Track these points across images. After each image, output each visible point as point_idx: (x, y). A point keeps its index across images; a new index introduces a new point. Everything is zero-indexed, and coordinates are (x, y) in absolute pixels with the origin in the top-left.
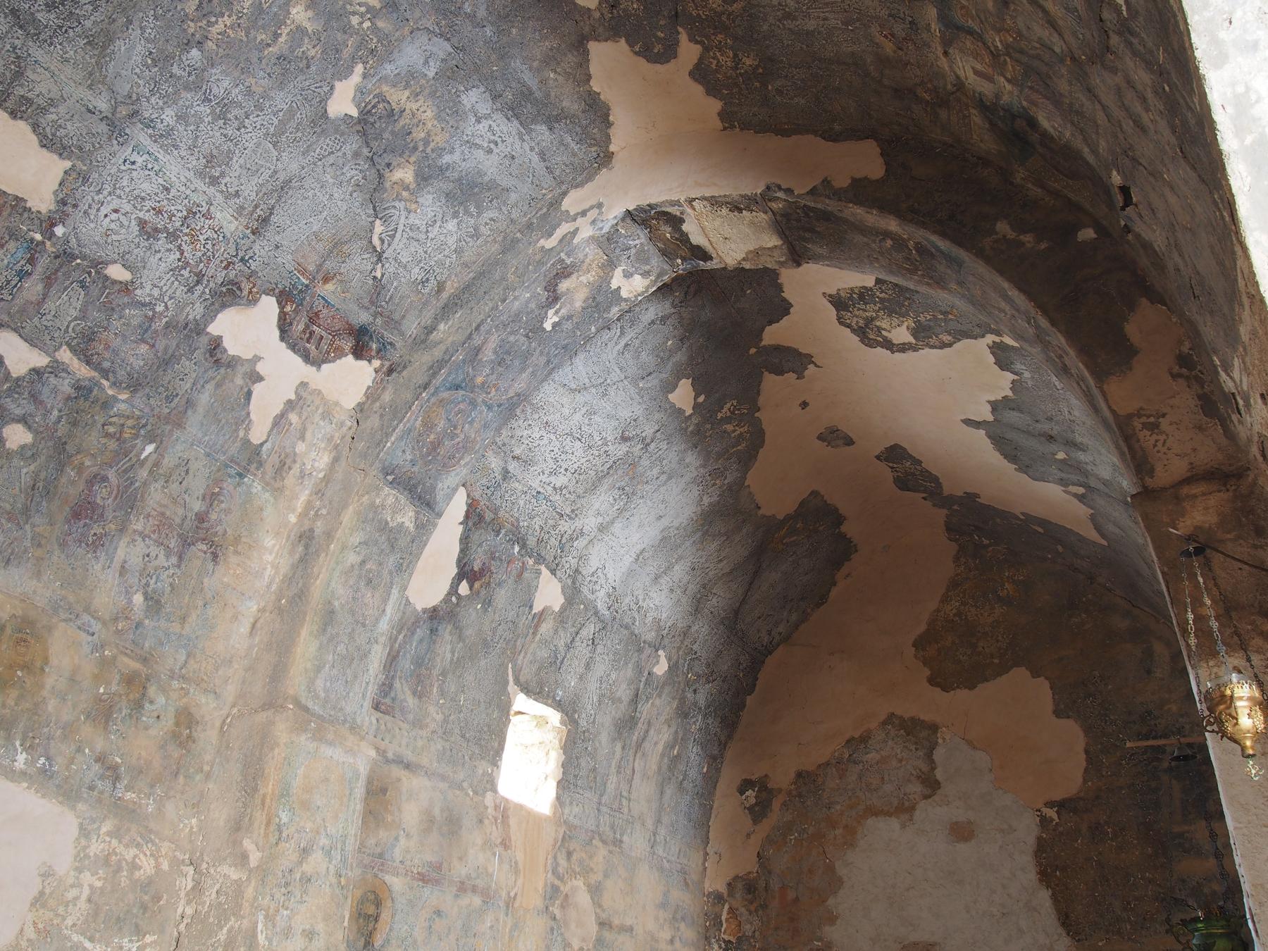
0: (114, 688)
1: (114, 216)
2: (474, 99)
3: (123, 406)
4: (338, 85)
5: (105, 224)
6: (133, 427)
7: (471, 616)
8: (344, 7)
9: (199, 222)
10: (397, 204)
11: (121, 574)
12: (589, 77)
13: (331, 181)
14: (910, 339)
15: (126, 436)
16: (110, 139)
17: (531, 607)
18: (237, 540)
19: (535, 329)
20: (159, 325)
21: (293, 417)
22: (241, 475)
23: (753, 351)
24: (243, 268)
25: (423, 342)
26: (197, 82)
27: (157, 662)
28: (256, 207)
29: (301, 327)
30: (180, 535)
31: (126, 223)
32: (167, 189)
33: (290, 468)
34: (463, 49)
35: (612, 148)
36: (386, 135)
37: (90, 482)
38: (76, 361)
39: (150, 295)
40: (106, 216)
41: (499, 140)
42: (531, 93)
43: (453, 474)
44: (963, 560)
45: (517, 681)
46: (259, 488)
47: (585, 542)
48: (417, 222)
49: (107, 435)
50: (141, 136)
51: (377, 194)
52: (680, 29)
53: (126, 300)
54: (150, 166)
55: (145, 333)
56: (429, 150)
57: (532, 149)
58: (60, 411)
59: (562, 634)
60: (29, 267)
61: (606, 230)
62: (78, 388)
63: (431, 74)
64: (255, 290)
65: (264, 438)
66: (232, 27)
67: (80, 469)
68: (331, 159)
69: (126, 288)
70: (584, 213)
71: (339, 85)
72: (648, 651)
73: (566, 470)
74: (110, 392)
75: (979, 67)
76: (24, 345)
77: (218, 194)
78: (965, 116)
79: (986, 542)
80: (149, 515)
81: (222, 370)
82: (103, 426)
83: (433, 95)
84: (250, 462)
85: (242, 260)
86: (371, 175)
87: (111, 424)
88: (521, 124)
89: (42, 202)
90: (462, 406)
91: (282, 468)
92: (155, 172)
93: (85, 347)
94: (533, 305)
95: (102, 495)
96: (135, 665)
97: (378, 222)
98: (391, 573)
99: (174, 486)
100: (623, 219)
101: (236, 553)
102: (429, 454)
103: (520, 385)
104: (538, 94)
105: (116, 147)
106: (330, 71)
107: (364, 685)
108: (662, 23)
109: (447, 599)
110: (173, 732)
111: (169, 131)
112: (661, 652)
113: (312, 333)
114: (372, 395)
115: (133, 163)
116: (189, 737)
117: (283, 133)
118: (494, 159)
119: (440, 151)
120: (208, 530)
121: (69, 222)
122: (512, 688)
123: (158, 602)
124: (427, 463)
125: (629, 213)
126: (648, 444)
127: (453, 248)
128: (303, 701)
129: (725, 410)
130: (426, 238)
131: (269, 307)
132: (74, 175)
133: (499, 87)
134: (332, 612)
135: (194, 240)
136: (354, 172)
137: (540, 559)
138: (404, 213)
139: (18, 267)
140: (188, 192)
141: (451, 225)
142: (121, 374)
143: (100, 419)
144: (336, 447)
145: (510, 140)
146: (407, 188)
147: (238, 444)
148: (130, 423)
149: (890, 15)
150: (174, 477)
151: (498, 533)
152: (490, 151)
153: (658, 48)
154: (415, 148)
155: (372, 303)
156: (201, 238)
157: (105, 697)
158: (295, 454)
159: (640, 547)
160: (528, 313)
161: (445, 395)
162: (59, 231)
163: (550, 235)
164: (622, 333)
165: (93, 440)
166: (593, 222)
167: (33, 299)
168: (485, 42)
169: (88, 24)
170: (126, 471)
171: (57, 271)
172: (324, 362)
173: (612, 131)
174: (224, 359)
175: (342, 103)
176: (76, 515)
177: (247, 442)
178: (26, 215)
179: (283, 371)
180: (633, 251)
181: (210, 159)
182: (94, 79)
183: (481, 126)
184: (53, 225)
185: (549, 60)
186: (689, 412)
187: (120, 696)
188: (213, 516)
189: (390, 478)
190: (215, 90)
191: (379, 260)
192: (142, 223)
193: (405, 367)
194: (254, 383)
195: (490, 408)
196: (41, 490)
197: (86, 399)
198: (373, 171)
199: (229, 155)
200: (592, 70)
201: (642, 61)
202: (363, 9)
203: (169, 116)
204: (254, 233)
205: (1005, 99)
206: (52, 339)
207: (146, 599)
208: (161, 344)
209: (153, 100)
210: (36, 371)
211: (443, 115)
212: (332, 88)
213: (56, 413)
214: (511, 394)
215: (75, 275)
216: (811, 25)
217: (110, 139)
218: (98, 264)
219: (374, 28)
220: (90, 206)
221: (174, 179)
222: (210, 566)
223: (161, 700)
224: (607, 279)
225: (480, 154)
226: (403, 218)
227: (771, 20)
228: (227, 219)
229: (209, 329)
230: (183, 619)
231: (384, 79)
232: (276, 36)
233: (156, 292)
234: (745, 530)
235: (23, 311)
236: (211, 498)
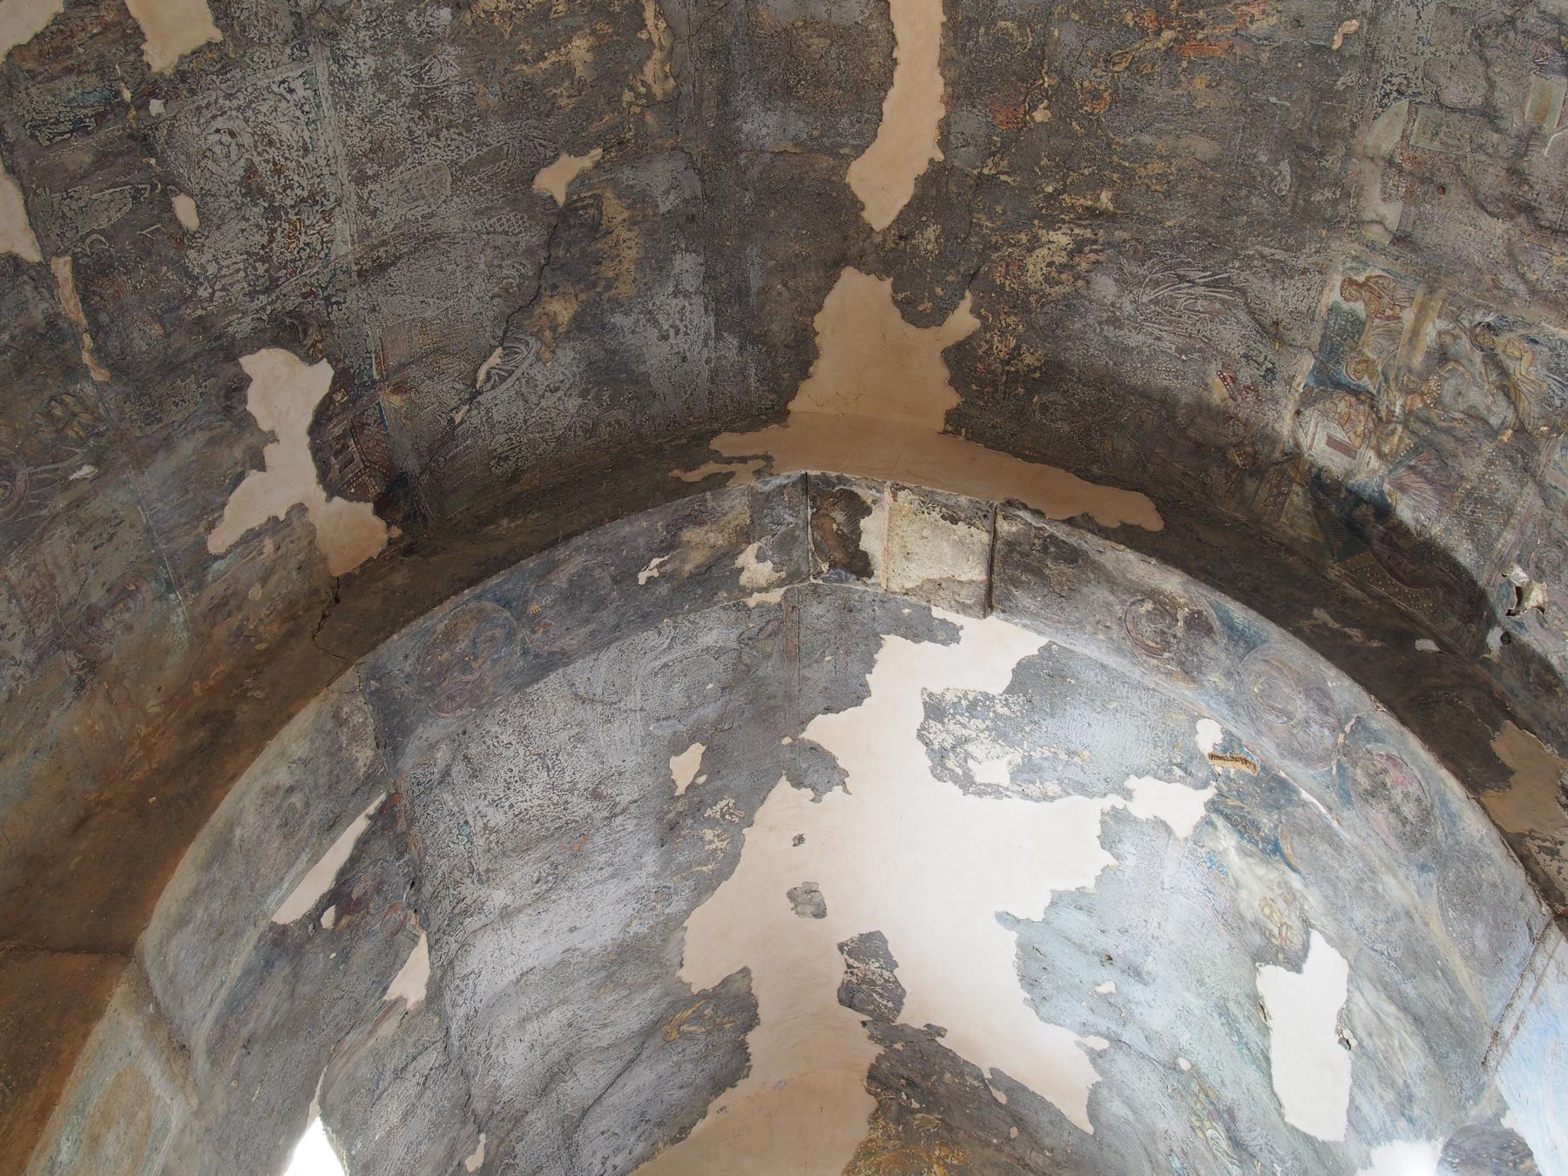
1: (226, 138)
2: (686, 266)
3: (89, 389)
4: (564, 158)
5: (213, 141)
6: (84, 427)
7: (319, 960)
8: (626, 74)
9: (312, 217)
10: (532, 341)
13: (482, 266)
14: (1005, 780)
15: (71, 433)
16: (286, 42)
17: (386, 989)
20: (191, 312)
22: (170, 587)
23: (787, 741)
28: (384, 243)
29: (338, 431)
30: (56, 624)
31: (234, 157)
32: (306, 150)
33: (229, 615)
34: (711, 201)
38: (70, 285)
39: (202, 267)
40: (218, 131)
44: (882, 1122)
45: (322, 1103)
46: (181, 619)
47: (478, 925)
49: (49, 415)
52: (968, 294)
53: (172, 253)
54: (306, 108)
58: (12, 338)
59: (397, 1050)
63: (663, 209)
64: (320, 346)
66: (502, 14)
69: (182, 238)
71: (564, 158)
72: (471, 1127)
73: (511, 806)
75: (1340, 435)
76: (21, 217)
77: (354, 197)
78: (1280, 493)
79: (915, 1105)
81: (227, 425)
82: (52, 398)
85: (327, 298)
87: (62, 403)
88: (716, 324)
89: (160, 57)
93: (90, 277)
98: (312, 826)
99: (86, 547)
100: (794, 484)
103: (570, 642)
104: (753, 300)
105: (285, 59)
107: (217, 984)
108: (950, 278)
109: (301, 923)
111: (357, 82)
112: (482, 1137)
113: (345, 447)
114: (370, 569)
115: (291, 91)
117: (472, 174)
118: (664, 349)
119: (616, 304)
122: (314, 1106)
126: (615, 815)
127: (558, 433)
129: (718, 808)
132: (216, 55)
133: (720, 268)
134: (228, 843)
135: (291, 236)
136: (513, 272)
137: (425, 923)
138: (531, 358)
139: (81, 113)
140: (326, 171)
142: (114, 344)
145: (693, 337)
146: (554, 329)
149: (1246, 356)
151: (401, 855)
152: (665, 338)
153: (926, 306)
154: (594, 285)
156: (303, 238)
158: (245, 598)
159: (530, 963)
161: (489, 605)
163: (692, 469)
164: (670, 647)
170: (42, 483)
171: (121, 154)
175: (554, 181)
177: (202, 544)
178: (132, 57)
180: (783, 529)
181: (377, 147)
183: (675, 301)
186: (680, 790)
188: (108, 624)
190: (435, 72)
191: (470, 400)
192: (251, 171)
194: (253, 467)
195: (525, 653)
198: (534, 284)
201: (896, 314)
202: (643, 90)
203: (367, 65)
204: (360, 274)
205: (1360, 479)
206: (61, 236)
212: (556, 157)
214: (556, 648)
216: (1135, 340)
217: (286, 42)
218: (171, 185)
219: (640, 119)
220: (208, 106)
221: (321, 143)
224: (734, 551)
226: (525, 365)
227: (1091, 319)
229: (244, 360)
231: (615, 183)
233: (212, 269)
234: (650, 992)
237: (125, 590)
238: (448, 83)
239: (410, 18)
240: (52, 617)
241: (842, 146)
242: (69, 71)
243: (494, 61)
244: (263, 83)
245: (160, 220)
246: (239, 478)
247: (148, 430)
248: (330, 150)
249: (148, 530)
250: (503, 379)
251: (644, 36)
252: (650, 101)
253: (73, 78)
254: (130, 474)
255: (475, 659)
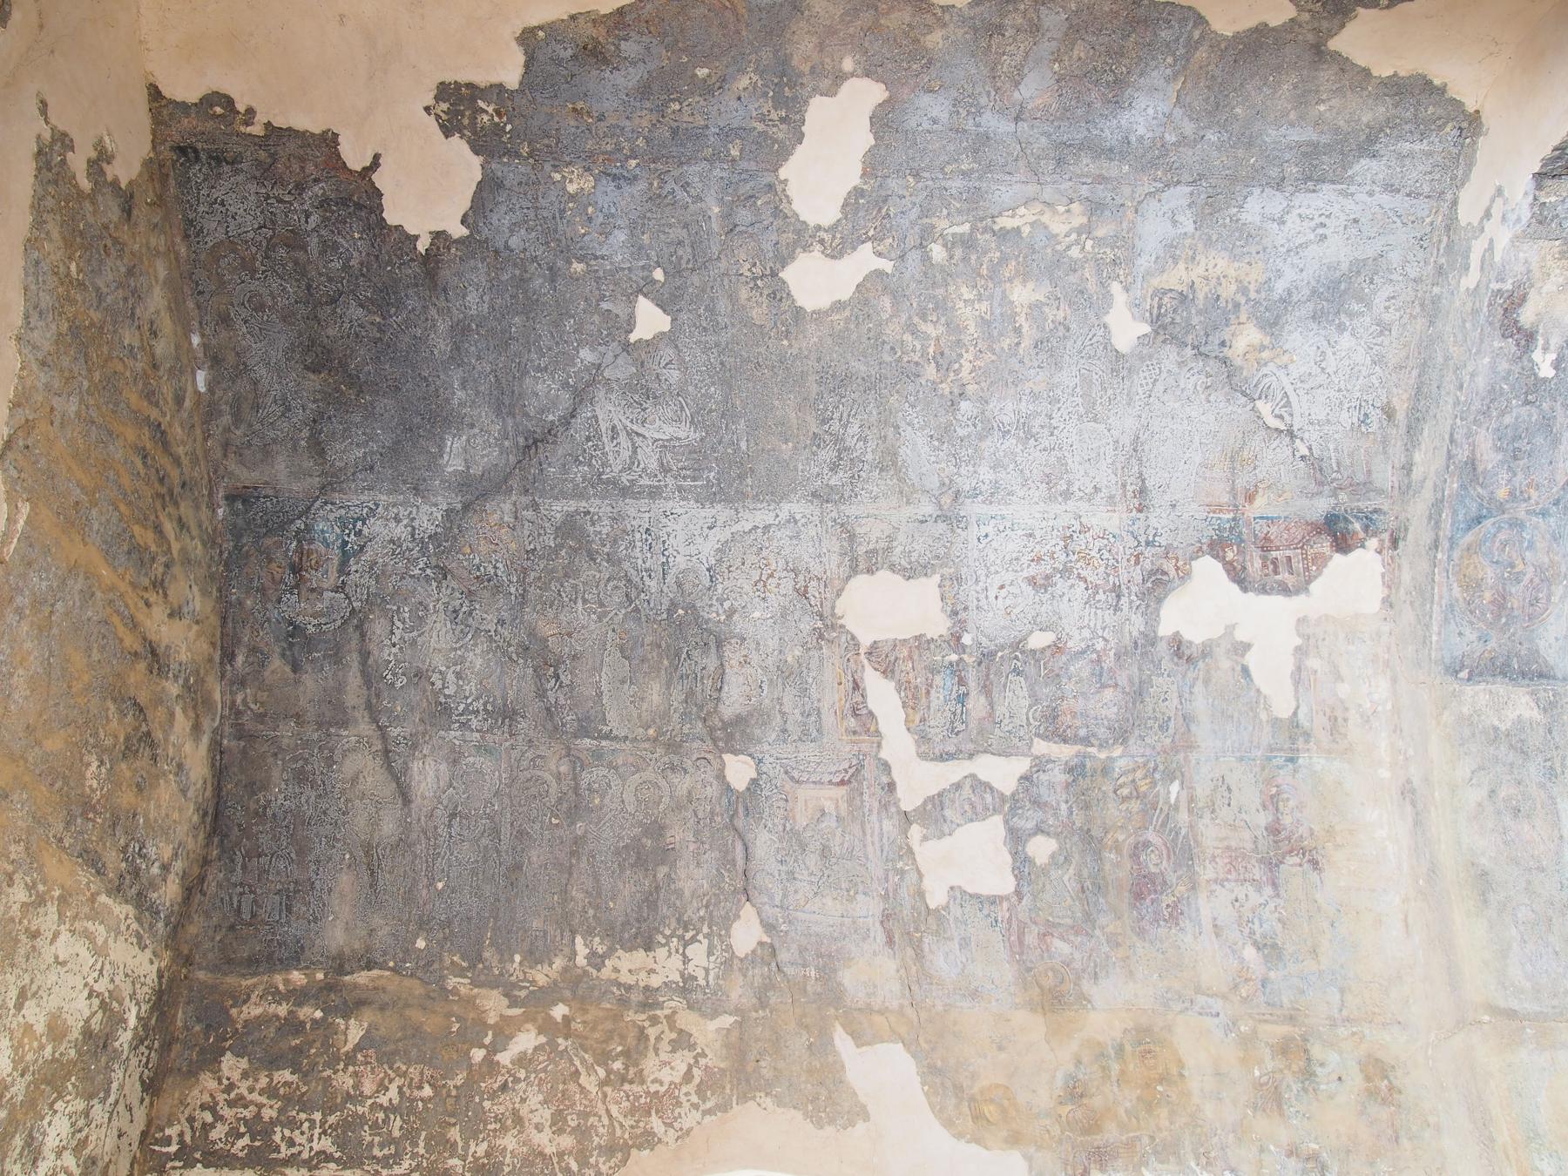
0: (1269, 1065)
1: (1003, 593)
4: (1108, 319)
6: (1145, 777)
9: (1080, 542)
10: (1265, 370)
11: (1217, 935)
12: (1366, 72)
13: (1177, 405)
15: (1143, 789)
16: (953, 531)
18: (1330, 832)
19: (1533, 388)
20: (1109, 661)
21: (1312, 663)
24: (1154, 550)
25: (1409, 486)
26: (986, 426)
27: (1307, 1016)
28: (1124, 486)
29: (1258, 563)
30: (1261, 861)
31: (1018, 591)
33: (1345, 720)
34: (1201, 176)
35: (1470, 108)
36: (1195, 321)
37: (1135, 856)
41: (1323, 219)
42: (1315, 145)
43: (1552, 619)
46: (1322, 761)
48: (1302, 370)
49: (1125, 799)
50: (972, 509)
51: (1235, 380)
55: (1101, 678)
56: (1253, 295)
57: (1371, 194)
60: (963, 689)
61: (1526, 215)
62: (1070, 770)
63: (1190, 228)
64: (1180, 563)
65: (1294, 705)
66: (976, 358)
67: (1117, 848)
68: (1160, 387)
69: (1057, 648)
70: (1488, 215)
74: (1103, 756)
80: (1214, 857)
81: (1201, 664)
83: (1209, 243)
84: (1293, 740)
85: (1148, 543)
86: (1213, 366)
87: (1121, 786)
88: (1333, 182)
89: (939, 626)
90: (1502, 536)
91: (1335, 725)
92: (1010, 529)
93: (1053, 726)
94: (1504, 366)
95: (1153, 862)
96: (1283, 1029)
97: (1259, 404)
98: (1542, 786)
100: (1539, 187)
101: (1337, 847)
102: (1500, 616)
104: (1325, 139)
105: (963, 534)
106: (1091, 315)
110: (1367, 1090)
111: (996, 485)
113: (1275, 562)
114: (1391, 583)
116: (1391, 1088)
120: (1289, 839)
121: (970, 626)
123: (1274, 946)
124: (1503, 630)
125: (1540, 177)
128: (1502, 1004)
130: (1324, 381)
131: (1208, 569)
132: (948, 583)
133: (1274, 172)
134: (1484, 874)
138: (1281, 374)
139: (954, 695)
141: (1346, 341)
142: (1102, 732)
143: (1108, 787)
144: (1387, 664)
145: (1336, 209)
146: (1263, 348)
147: (1267, 729)
148: (1139, 774)
150: (1218, 803)
152: (1323, 237)
154: (1237, 306)
155: (1321, 484)
156: (1093, 553)
157: (1264, 1079)
158: (1342, 702)
160: (1505, 379)
161: (1469, 538)
162: (967, 639)
165: (1114, 812)
166: (1504, 218)
167: (984, 714)
168: (1218, 149)
169: (869, 457)
170: (1164, 825)
172: (1308, 582)
173: (1452, 93)
174: (1195, 651)
176: (1138, 896)
177: (1276, 722)
179: (1267, 623)
181: (1048, 480)
182: (907, 495)
183: (1289, 224)
184: (959, 638)
185: (1303, 99)
187: (1281, 1071)
188: (1287, 821)
189: (1464, 674)
190: (1006, 420)
193: (1406, 530)
194: (1243, 656)
195: (1544, 514)
196: (1092, 888)
197: (1084, 777)
198: (1211, 362)
199: (1061, 461)
200: (1361, 61)
203: (986, 474)
204: (1140, 511)
207: (1259, 949)
208: (1122, 680)
209: (963, 471)
210: (1025, 778)
211: (1238, 251)
212: (1105, 326)
213: (1064, 806)
215: (1006, 669)
217: (953, 531)
218: (1018, 645)
219: (1100, 242)
222: (1314, 876)
223: (1333, 1058)
225: (1314, 250)
226: (1286, 381)
228: (1107, 519)
230: (1314, 952)
231: (1148, 274)
232: (1018, 331)
235: (981, 732)
236: (1273, 801)
237: (1272, 797)
238: (1017, 412)
239: (961, 432)
240: (1253, 861)
241: (1190, 37)
242: (928, 692)
243: (1011, 372)
244: (976, 554)
245: (1038, 661)
246: (1245, 671)
247: (1171, 731)
248: (1038, 515)
249: (1241, 759)
250: (1288, 404)
251: (1026, 230)
252: (1086, 230)
253: (933, 692)
254: (1193, 757)
255: (1512, 566)
